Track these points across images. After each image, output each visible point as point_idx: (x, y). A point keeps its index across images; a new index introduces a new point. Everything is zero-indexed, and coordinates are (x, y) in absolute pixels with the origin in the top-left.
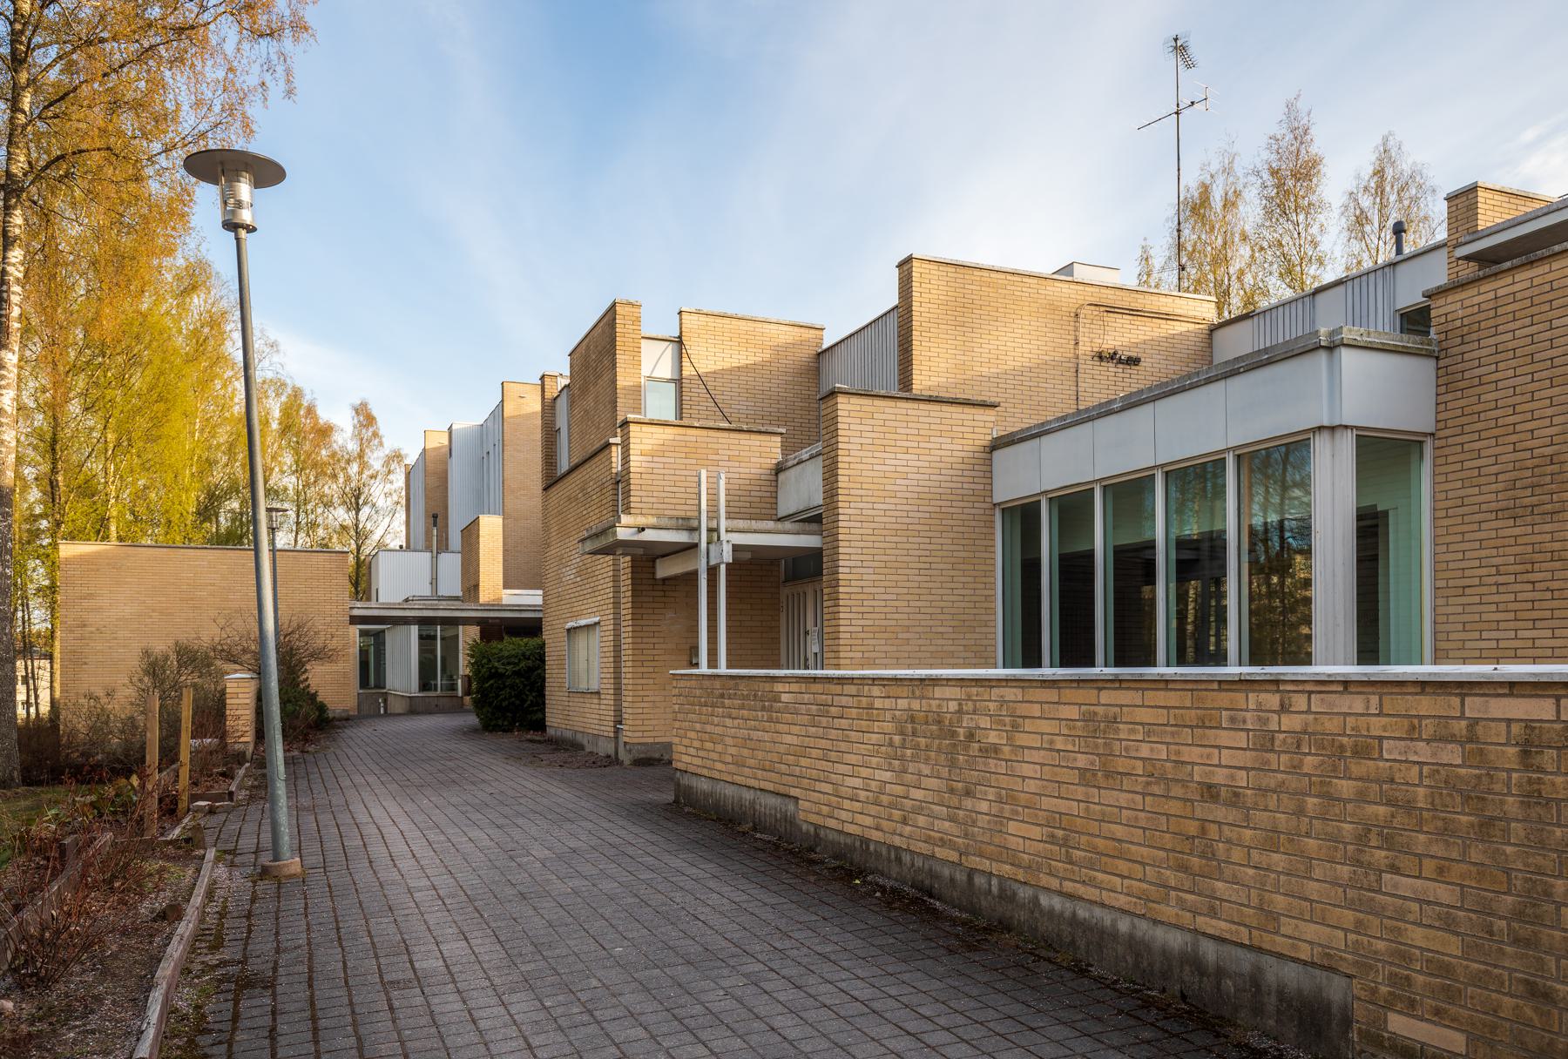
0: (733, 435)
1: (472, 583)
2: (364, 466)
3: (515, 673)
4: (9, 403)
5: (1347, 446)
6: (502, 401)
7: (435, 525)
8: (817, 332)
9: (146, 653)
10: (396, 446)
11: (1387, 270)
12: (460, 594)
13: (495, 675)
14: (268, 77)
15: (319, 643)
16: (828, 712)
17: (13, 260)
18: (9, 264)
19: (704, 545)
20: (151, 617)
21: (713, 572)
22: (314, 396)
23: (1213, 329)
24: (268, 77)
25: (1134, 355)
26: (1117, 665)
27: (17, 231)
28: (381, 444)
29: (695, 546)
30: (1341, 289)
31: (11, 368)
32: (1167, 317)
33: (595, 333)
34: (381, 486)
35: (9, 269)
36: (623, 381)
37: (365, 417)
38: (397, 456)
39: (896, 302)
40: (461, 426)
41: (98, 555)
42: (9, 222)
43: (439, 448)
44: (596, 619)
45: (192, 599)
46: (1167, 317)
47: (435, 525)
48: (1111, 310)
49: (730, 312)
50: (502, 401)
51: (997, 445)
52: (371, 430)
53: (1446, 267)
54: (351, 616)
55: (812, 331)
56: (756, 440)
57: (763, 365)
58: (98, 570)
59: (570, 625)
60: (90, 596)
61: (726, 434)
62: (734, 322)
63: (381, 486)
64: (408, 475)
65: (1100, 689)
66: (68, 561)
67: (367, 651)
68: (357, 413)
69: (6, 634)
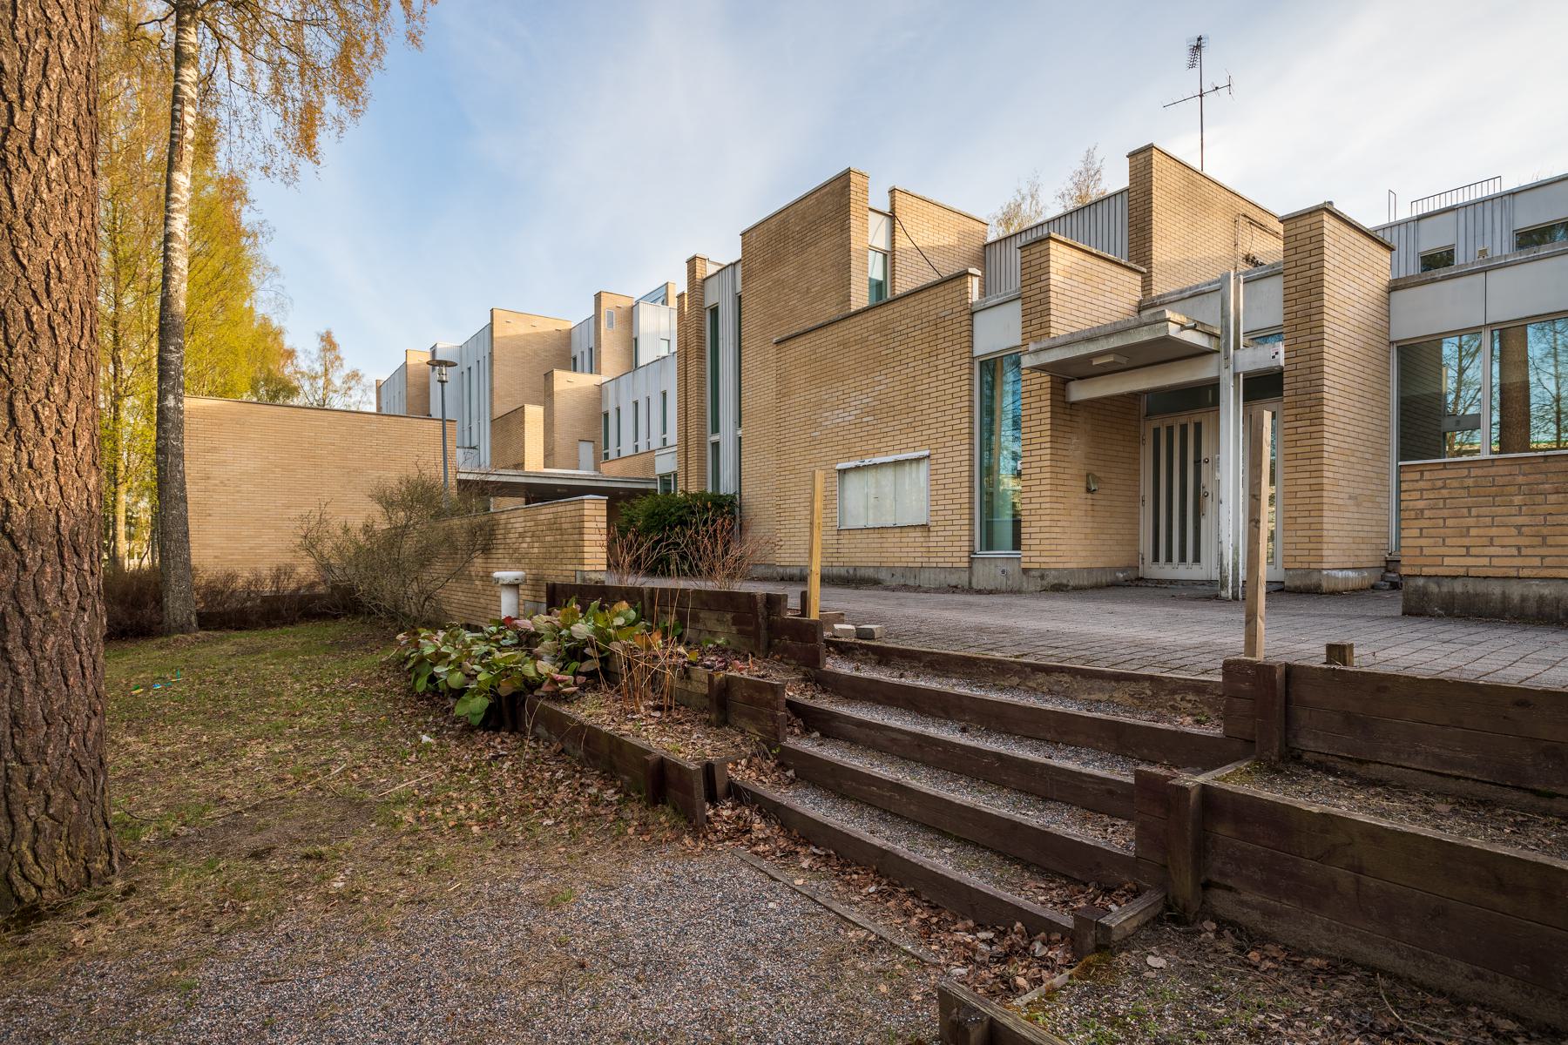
2: (328, 382)
4: (182, 228)
8: (984, 226)
10: (355, 367)
11: (1506, 198)
16: (1511, 501)
17: (187, 79)
18: (184, 82)
30: (1452, 215)
31: (184, 192)
33: (801, 206)
35: (184, 87)
37: (328, 343)
42: (184, 38)
43: (419, 365)
44: (926, 453)
45: (314, 457)
49: (928, 197)
50: (492, 323)
53: (1020, 314)
55: (981, 225)
58: (221, 425)
59: (839, 466)
60: (214, 450)
62: (931, 206)
69: (179, 472)
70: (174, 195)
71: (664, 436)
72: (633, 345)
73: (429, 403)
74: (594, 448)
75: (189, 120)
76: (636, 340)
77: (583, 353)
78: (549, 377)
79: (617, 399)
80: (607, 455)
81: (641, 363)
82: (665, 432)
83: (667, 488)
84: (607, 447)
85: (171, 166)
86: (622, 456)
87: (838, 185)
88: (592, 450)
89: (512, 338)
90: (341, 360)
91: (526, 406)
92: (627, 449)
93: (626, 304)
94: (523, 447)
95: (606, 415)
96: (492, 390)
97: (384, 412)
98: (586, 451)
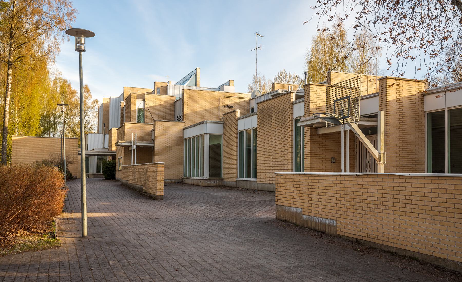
0: (144, 125)
1: (111, 145)
3: (112, 167)
5: (208, 136)
6: (124, 92)
7: (104, 127)
9: (37, 162)
10: (95, 99)
12: (108, 147)
13: (107, 167)
14: (64, 38)
15: (71, 160)
17: (10, 79)
18: (9, 80)
19: (132, 146)
20: (32, 153)
21: (134, 150)
22: (70, 82)
23: (250, 100)
24: (64, 38)
25: (232, 106)
26: (451, 173)
27: (11, 73)
28: (91, 97)
29: (131, 146)
32: (240, 98)
34: (91, 111)
36: (132, 109)
38: (96, 101)
41: (21, 139)
45: (41, 149)
46: (240, 98)
47: (104, 127)
48: (227, 97)
51: (185, 129)
54: (78, 154)
56: (148, 126)
57: (162, 105)
59: (119, 157)
61: (142, 125)
63: (91, 111)
64: (99, 109)
65: (322, 177)
66: (14, 140)
70: (6, 102)
75: (10, 87)
85: (6, 97)
87: (129, 97)
91: (113, 128)
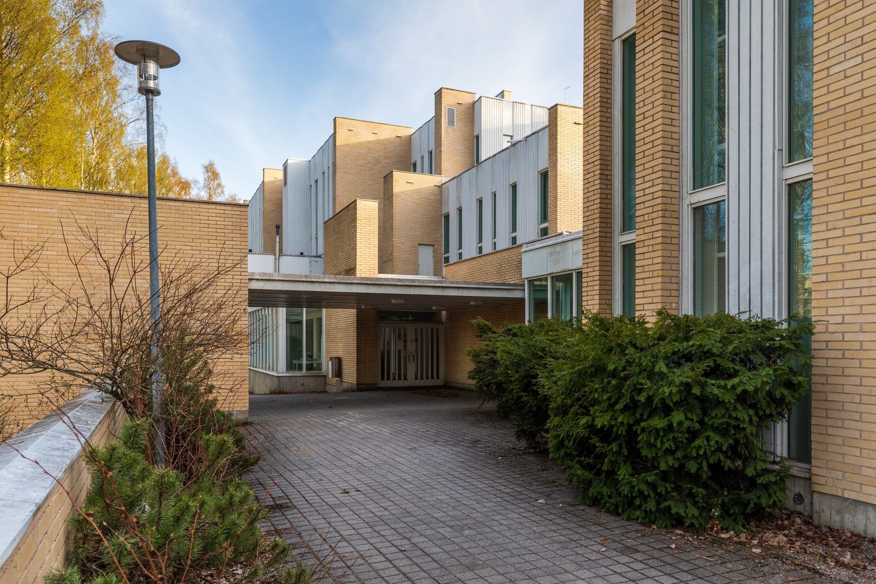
28: (223, 192)
37: (212, 172)
39: (547, 123)
40: (294, 161)
52: (216, 182)
67: (720, 29)
68: (207, 171)
71: (513, 235)
72: (475, 141)
73: (282, 216)
74: (434, 252)
76: (477, 137)
77: (422, 157)
78: (388, 179)
79: (459, 199)
80: (447, 260)
81: (484, 156)
82: (514, 229)
83: (540, 296)
84: (447, 250)
86: (498, 249)
88: (431, 254)
89: (354, 146)
90: (223, 187)
92: (470, 250)
93: (467, 99)
94: (355, 249)
95: (447, 217)
96: (334, 199)
97: (859, 378)
98: (426, 256)
